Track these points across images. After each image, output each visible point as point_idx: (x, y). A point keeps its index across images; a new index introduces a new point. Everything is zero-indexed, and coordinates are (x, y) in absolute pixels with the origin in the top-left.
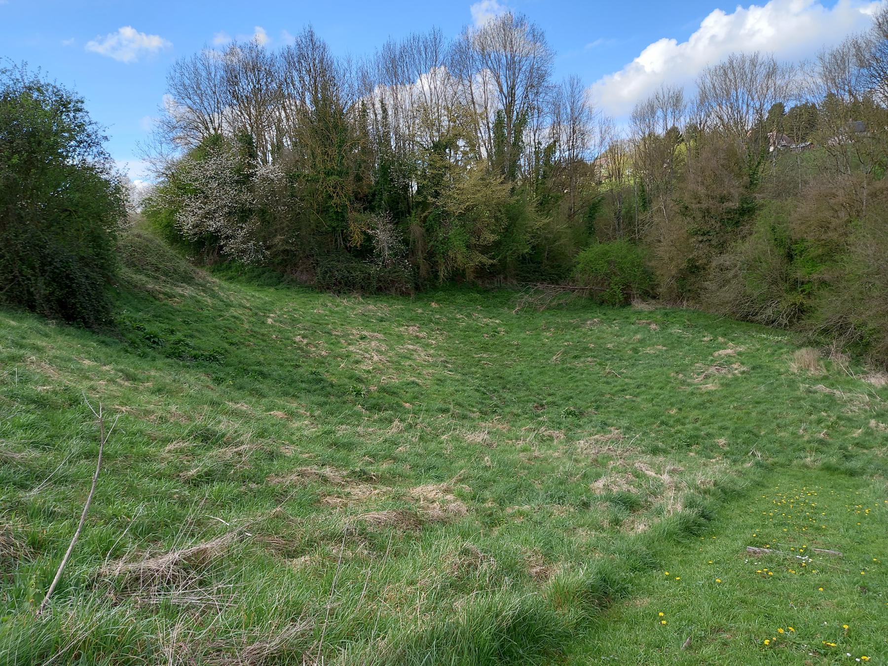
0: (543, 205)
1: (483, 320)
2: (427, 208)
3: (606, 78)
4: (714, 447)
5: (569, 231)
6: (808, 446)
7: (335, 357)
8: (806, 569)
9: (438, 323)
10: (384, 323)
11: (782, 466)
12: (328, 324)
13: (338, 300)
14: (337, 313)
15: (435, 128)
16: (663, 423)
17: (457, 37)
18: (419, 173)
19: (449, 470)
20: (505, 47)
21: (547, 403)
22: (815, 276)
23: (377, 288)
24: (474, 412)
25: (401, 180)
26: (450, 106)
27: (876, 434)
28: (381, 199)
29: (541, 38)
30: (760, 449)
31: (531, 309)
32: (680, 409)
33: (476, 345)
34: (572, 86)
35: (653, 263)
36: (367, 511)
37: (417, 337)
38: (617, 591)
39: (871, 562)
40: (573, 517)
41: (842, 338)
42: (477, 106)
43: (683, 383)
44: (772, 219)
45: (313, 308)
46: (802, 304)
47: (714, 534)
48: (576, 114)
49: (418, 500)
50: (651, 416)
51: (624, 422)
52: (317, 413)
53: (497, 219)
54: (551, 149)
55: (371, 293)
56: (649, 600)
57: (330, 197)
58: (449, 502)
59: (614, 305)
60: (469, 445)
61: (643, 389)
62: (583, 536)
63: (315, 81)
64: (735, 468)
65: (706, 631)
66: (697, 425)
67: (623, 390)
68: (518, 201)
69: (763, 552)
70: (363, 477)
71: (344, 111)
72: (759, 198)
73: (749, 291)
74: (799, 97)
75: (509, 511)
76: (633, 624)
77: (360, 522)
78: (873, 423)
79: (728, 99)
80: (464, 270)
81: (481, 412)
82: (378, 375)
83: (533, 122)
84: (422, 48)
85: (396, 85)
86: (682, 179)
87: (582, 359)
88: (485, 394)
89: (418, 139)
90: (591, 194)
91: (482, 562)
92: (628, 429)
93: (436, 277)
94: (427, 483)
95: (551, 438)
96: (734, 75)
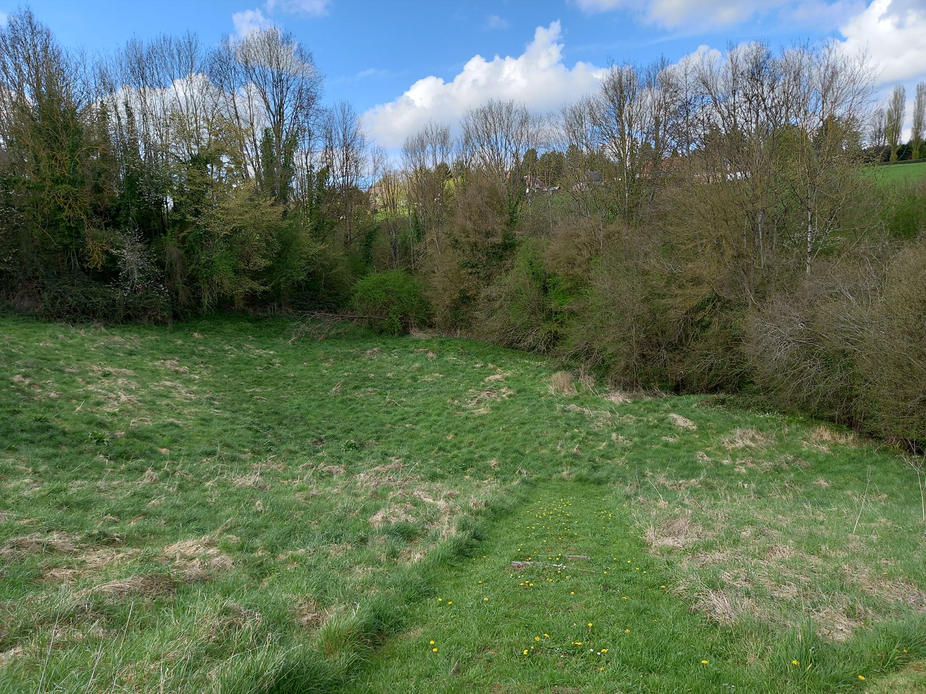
0: (318, 231)
1: (255, 351)
2: (186, 228)
3: (378, 108)
4: (487, 468)
5: (346, 258)
6: (564, 461)
7: (69, 399)
8: (559, 575)
9: (202, 356)
10: (134, 357)
11: (544, 481)
12: (58, 360)
13: (73, 331)
14: (71, 346)
15: (193, 140)
16: (440, 449)
17: (217, 45)
18: (175, 188)
19: (213, 519)
20: (271, 63)
21: (326, 438)
22: (566, 307)
23: (126, 317)
24: (245, 453)
25: (153, 194)
26: (210, 118)
27: (617, 445)
28: (128, 215)
29: (309, 60)
30: (525, 467)
31: (309, 339)
32: (456, 434)
33: (248, 379)
34: (343, 112)
35: (428, 293)
36: (107, 580)
37: (177, 372)
38: (391, 626)
39: (611, 562)
40: (350, 555)
41: (588, 362)
42: (241, 121)
43: (459, 408)
44: (530, 256)
45: (38, 341)
46: (556, 332)
47: (485, 554)
48: (349, 141)
49: (173, 559)
50: (429, 443)
51: (405, 451)
52: (42, 468)
53: (268, 243)
54: (324, 174)
55: (116, 322)
56: (422, 630)
57: (60, 209)
58: (210, 557)
59: (393, 334)
60: (238, 490)
61: (422, 416)
62: (360, 573)
63: (37, 71)
64: (504, 487)
65: (473, 651)
66: (472, 448)
67: (403, 419)
68: (291, 225)
69: (525, 564)
70: (105, 540)
71: (78, 111)
72: (518, 235)
73: (512, 321)
74: (547, 145)
75: (282, 557)
76: (406, 658)
77: (95, 595)
78: (614, 435)
79: (489, 142)
80: (232, 297)
81: (254, 453)
82: (127, 418)
83: (304, 145)
84: (175, 51)
85: (144, 87)
86: (452, 213)
87: (362, 390)
88: (257, 431)
89: (174, 151)
90: (367, 222)
91: (245, 620)
92: (408, 457)
93: (199, 303)
94: (185, 538)
95: (330, 474)
96: (494, 119)
